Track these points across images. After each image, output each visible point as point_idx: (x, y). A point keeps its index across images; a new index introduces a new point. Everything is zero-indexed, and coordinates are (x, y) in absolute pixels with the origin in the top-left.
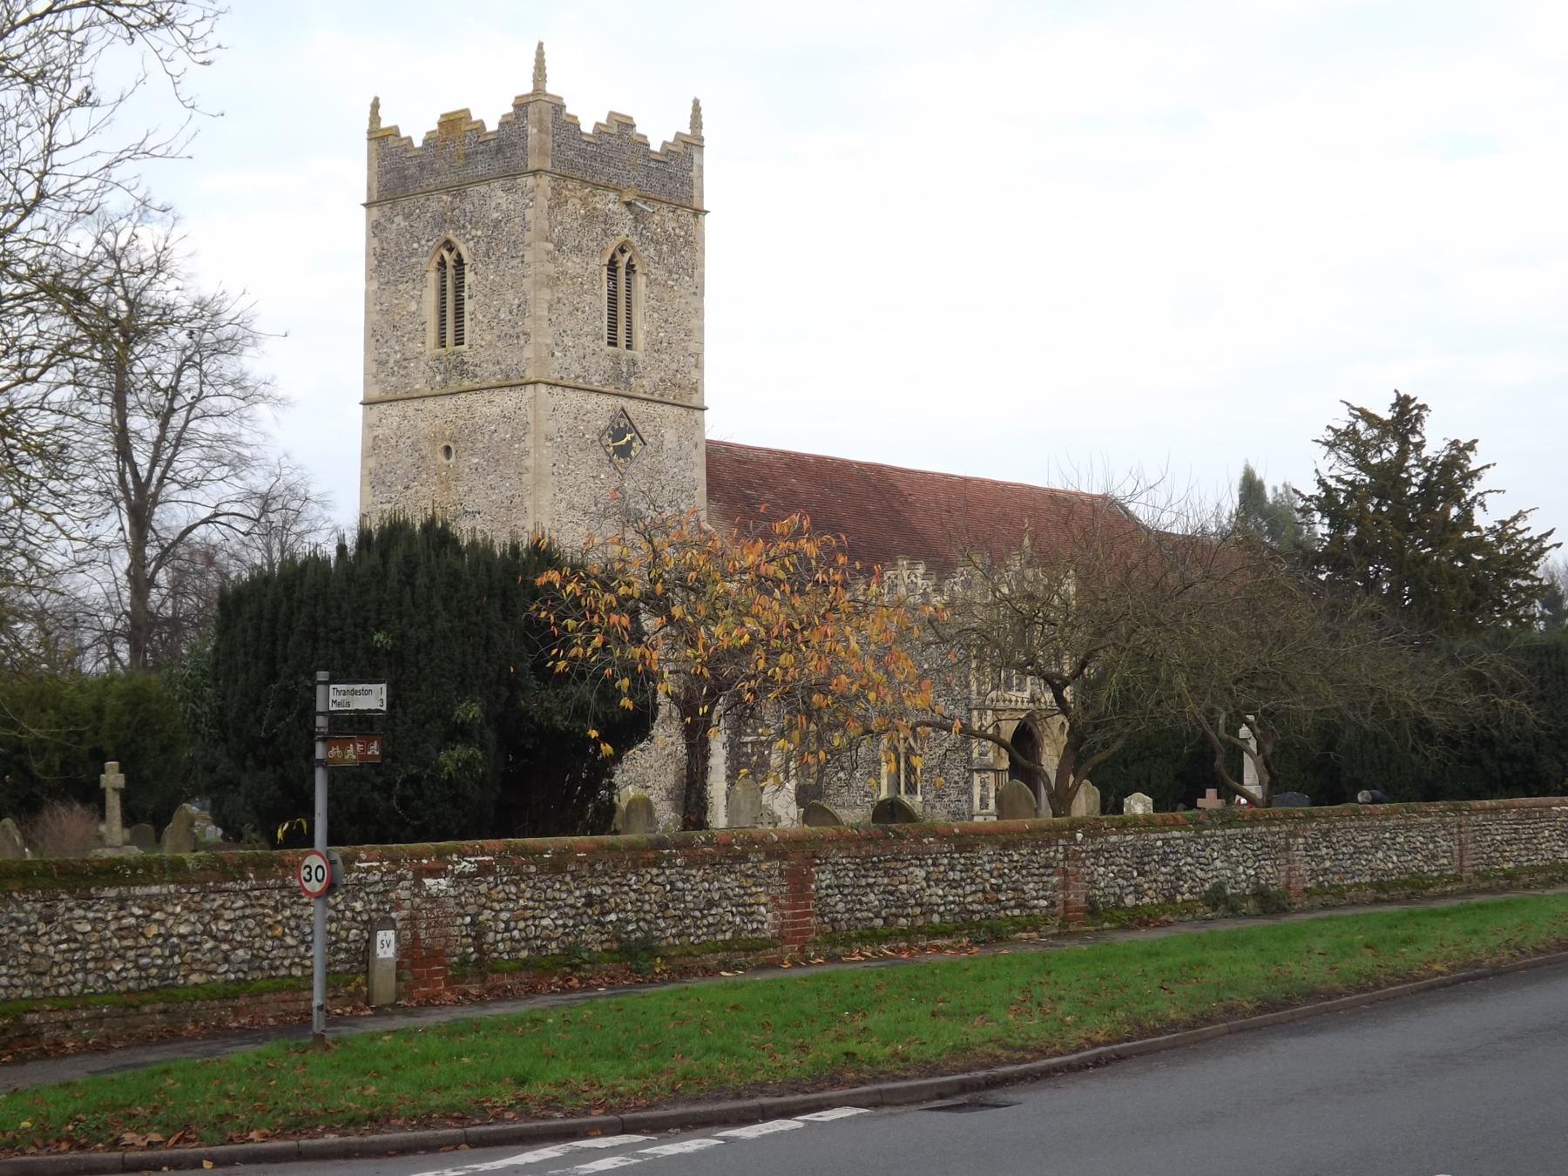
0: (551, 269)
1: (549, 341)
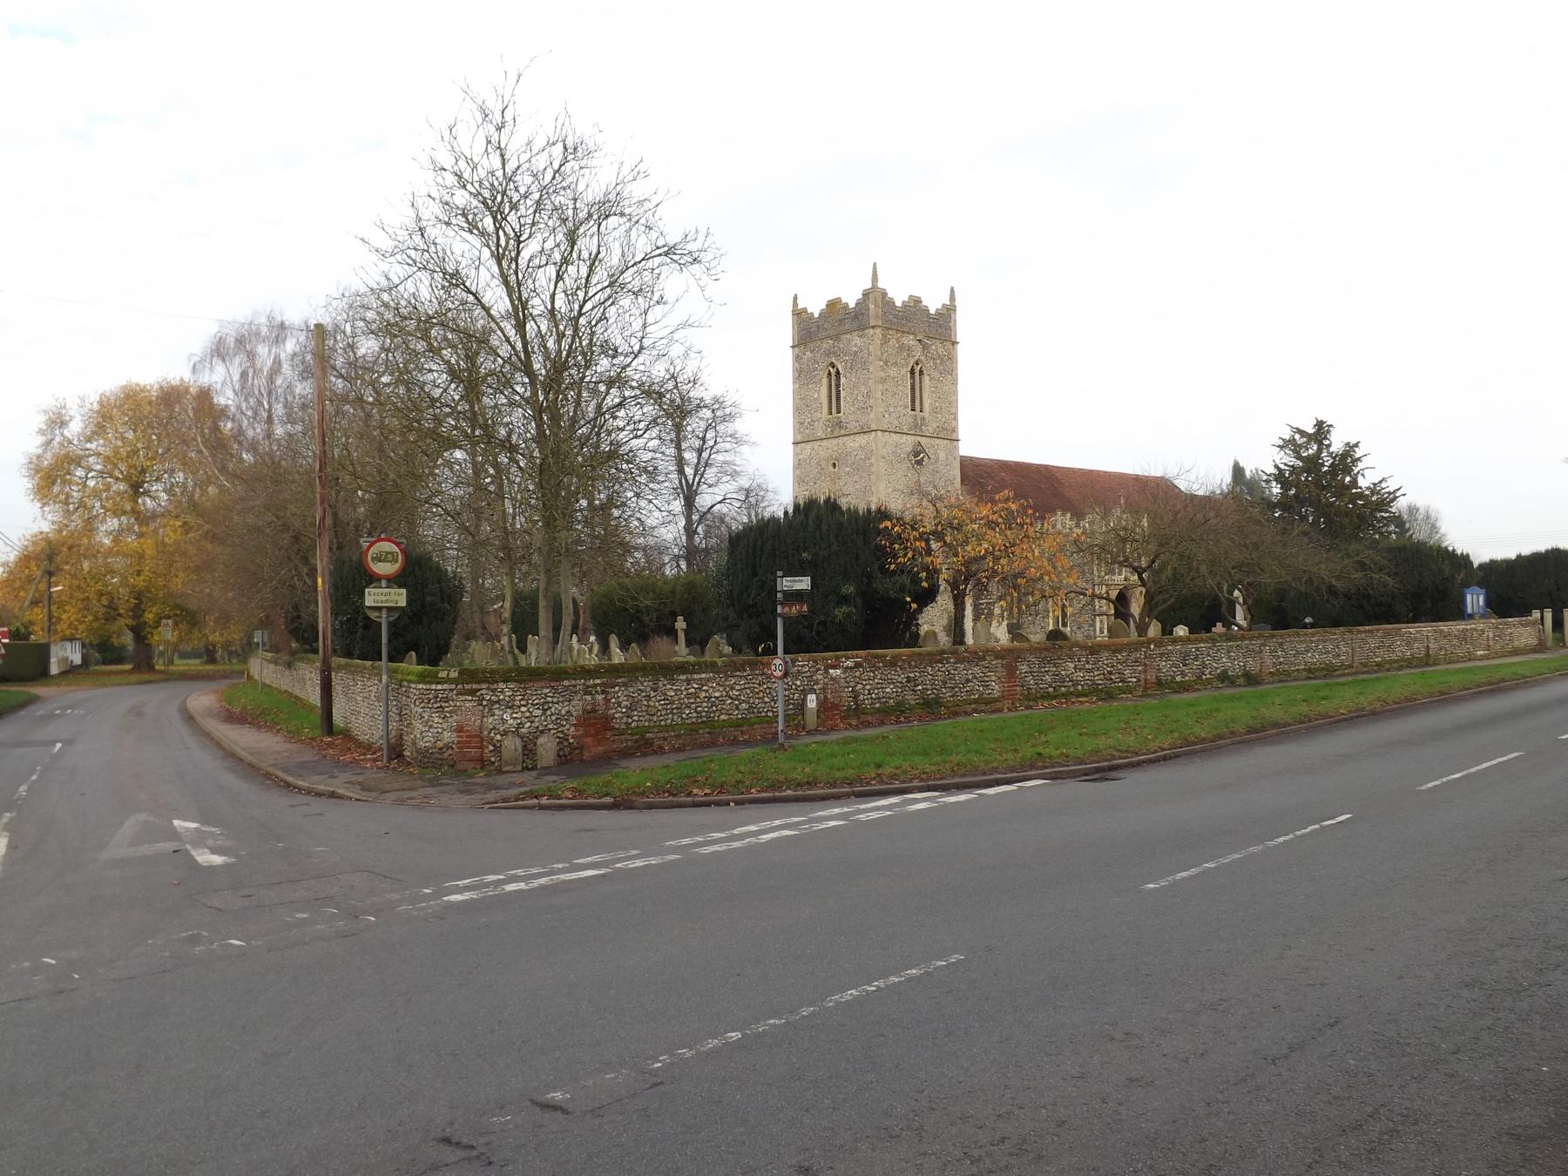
0: (882, 374)
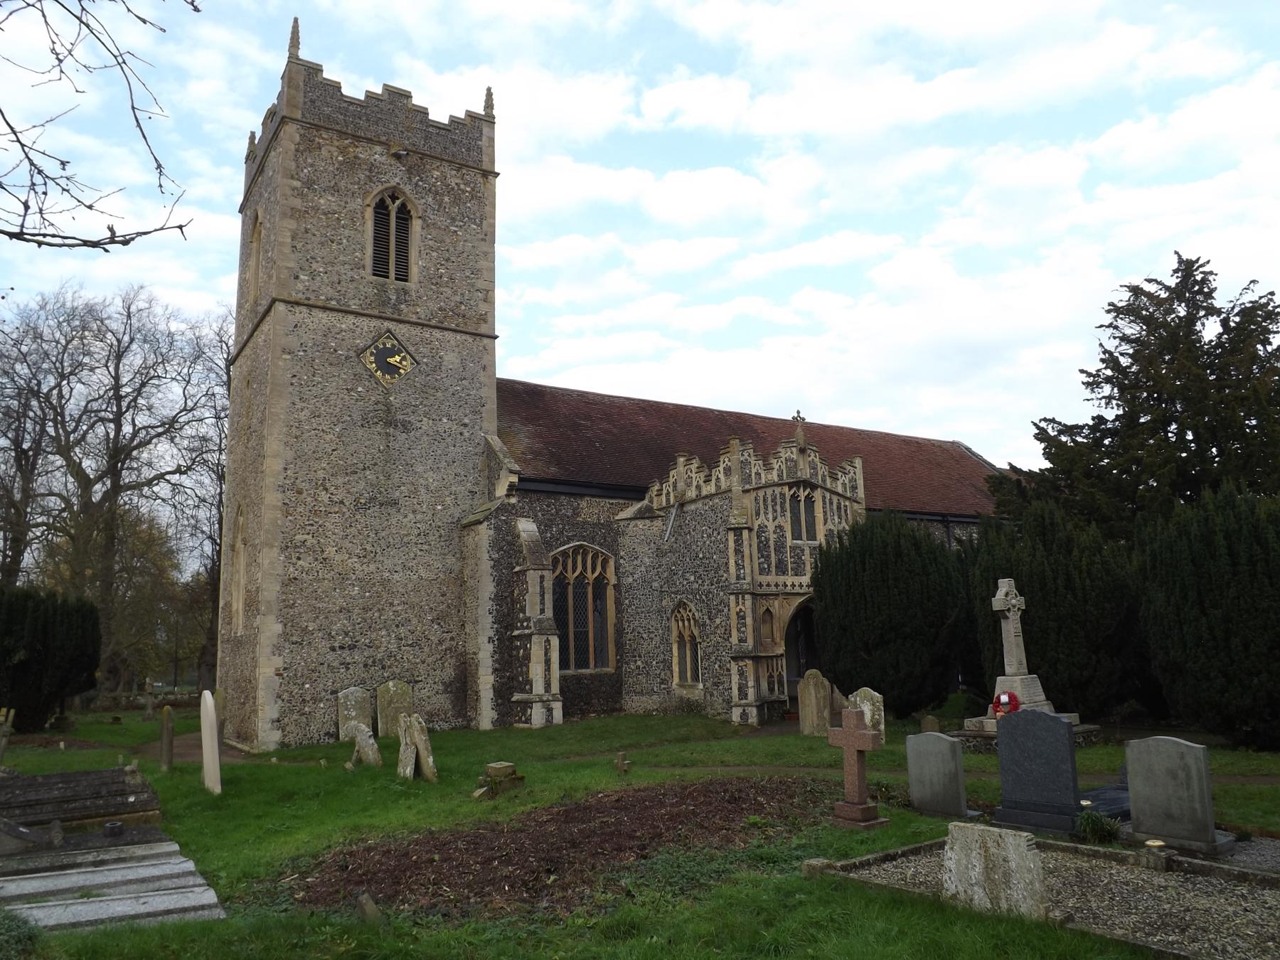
0: (297, 203)
1: (291, 265)
